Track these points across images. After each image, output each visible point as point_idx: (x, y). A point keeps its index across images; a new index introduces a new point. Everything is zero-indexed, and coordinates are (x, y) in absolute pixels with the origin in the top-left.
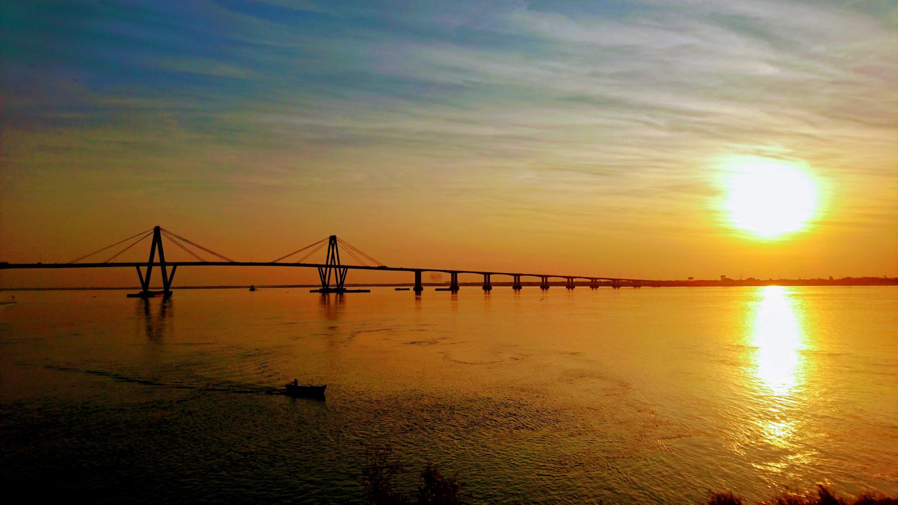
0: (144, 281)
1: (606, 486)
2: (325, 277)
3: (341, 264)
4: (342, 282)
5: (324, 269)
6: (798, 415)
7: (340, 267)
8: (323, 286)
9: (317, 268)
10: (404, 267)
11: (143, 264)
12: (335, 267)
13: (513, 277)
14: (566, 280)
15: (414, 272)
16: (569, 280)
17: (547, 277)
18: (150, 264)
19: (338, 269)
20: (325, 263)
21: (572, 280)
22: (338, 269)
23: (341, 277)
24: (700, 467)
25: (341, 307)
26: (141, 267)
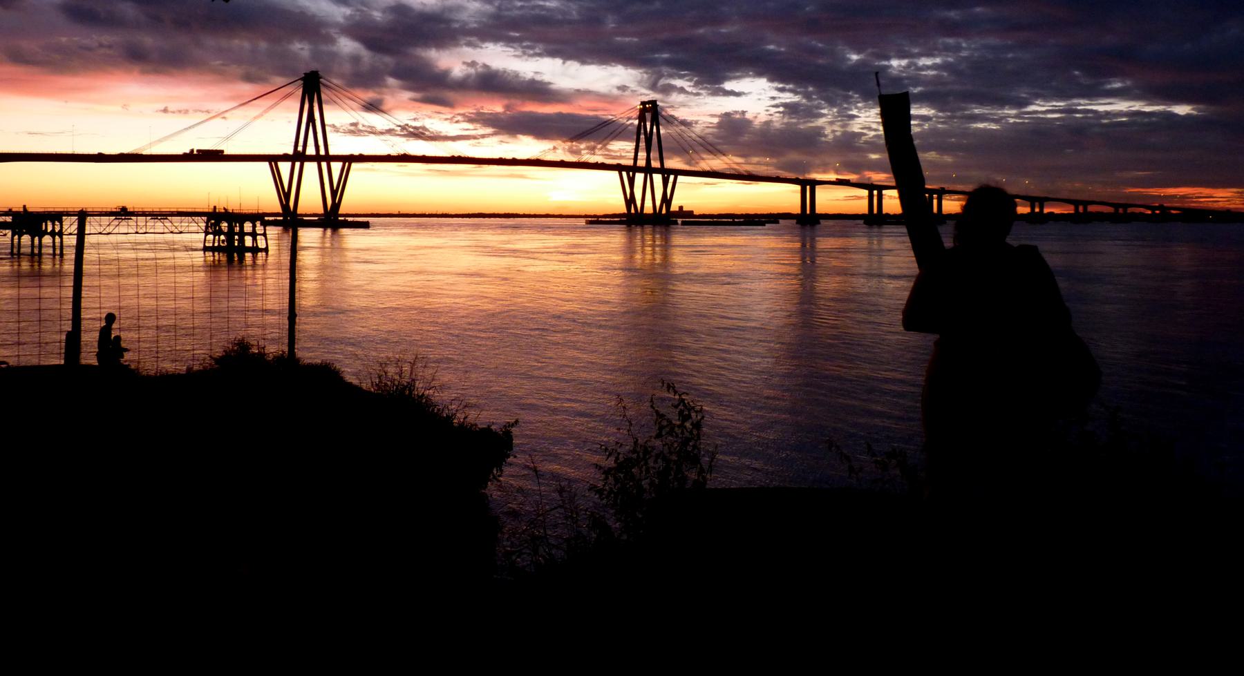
0: (286, 191)
1: (613, 365)
2: (287, 195)
3: (332, 152)
4: (336, 206)
5: (284, 167)
6: (719, 116)
7: (329, 158)
8: (628, 207)
9: (266, 164)
10: (366, 153)
11: (285, 158)
12: (317, 158)
13: (798, 188)
14: (1110, 210)
15: (679, 177)
16: (1076, 209)
17: (1086, 203)
18: (298, 157)
19: (324, 165)
20: (290, 152)
21: (1085, 209)
22: (324, 165)
23: (334, 193)
24: (689, 363)
25: (105, 332)
26: (281, 164)
